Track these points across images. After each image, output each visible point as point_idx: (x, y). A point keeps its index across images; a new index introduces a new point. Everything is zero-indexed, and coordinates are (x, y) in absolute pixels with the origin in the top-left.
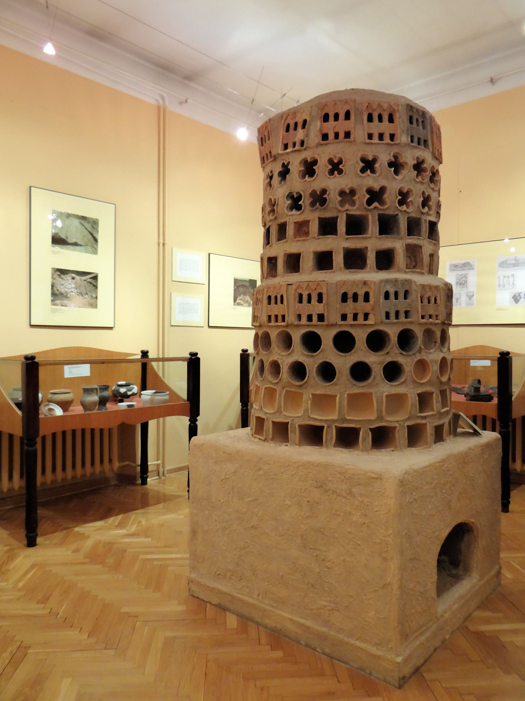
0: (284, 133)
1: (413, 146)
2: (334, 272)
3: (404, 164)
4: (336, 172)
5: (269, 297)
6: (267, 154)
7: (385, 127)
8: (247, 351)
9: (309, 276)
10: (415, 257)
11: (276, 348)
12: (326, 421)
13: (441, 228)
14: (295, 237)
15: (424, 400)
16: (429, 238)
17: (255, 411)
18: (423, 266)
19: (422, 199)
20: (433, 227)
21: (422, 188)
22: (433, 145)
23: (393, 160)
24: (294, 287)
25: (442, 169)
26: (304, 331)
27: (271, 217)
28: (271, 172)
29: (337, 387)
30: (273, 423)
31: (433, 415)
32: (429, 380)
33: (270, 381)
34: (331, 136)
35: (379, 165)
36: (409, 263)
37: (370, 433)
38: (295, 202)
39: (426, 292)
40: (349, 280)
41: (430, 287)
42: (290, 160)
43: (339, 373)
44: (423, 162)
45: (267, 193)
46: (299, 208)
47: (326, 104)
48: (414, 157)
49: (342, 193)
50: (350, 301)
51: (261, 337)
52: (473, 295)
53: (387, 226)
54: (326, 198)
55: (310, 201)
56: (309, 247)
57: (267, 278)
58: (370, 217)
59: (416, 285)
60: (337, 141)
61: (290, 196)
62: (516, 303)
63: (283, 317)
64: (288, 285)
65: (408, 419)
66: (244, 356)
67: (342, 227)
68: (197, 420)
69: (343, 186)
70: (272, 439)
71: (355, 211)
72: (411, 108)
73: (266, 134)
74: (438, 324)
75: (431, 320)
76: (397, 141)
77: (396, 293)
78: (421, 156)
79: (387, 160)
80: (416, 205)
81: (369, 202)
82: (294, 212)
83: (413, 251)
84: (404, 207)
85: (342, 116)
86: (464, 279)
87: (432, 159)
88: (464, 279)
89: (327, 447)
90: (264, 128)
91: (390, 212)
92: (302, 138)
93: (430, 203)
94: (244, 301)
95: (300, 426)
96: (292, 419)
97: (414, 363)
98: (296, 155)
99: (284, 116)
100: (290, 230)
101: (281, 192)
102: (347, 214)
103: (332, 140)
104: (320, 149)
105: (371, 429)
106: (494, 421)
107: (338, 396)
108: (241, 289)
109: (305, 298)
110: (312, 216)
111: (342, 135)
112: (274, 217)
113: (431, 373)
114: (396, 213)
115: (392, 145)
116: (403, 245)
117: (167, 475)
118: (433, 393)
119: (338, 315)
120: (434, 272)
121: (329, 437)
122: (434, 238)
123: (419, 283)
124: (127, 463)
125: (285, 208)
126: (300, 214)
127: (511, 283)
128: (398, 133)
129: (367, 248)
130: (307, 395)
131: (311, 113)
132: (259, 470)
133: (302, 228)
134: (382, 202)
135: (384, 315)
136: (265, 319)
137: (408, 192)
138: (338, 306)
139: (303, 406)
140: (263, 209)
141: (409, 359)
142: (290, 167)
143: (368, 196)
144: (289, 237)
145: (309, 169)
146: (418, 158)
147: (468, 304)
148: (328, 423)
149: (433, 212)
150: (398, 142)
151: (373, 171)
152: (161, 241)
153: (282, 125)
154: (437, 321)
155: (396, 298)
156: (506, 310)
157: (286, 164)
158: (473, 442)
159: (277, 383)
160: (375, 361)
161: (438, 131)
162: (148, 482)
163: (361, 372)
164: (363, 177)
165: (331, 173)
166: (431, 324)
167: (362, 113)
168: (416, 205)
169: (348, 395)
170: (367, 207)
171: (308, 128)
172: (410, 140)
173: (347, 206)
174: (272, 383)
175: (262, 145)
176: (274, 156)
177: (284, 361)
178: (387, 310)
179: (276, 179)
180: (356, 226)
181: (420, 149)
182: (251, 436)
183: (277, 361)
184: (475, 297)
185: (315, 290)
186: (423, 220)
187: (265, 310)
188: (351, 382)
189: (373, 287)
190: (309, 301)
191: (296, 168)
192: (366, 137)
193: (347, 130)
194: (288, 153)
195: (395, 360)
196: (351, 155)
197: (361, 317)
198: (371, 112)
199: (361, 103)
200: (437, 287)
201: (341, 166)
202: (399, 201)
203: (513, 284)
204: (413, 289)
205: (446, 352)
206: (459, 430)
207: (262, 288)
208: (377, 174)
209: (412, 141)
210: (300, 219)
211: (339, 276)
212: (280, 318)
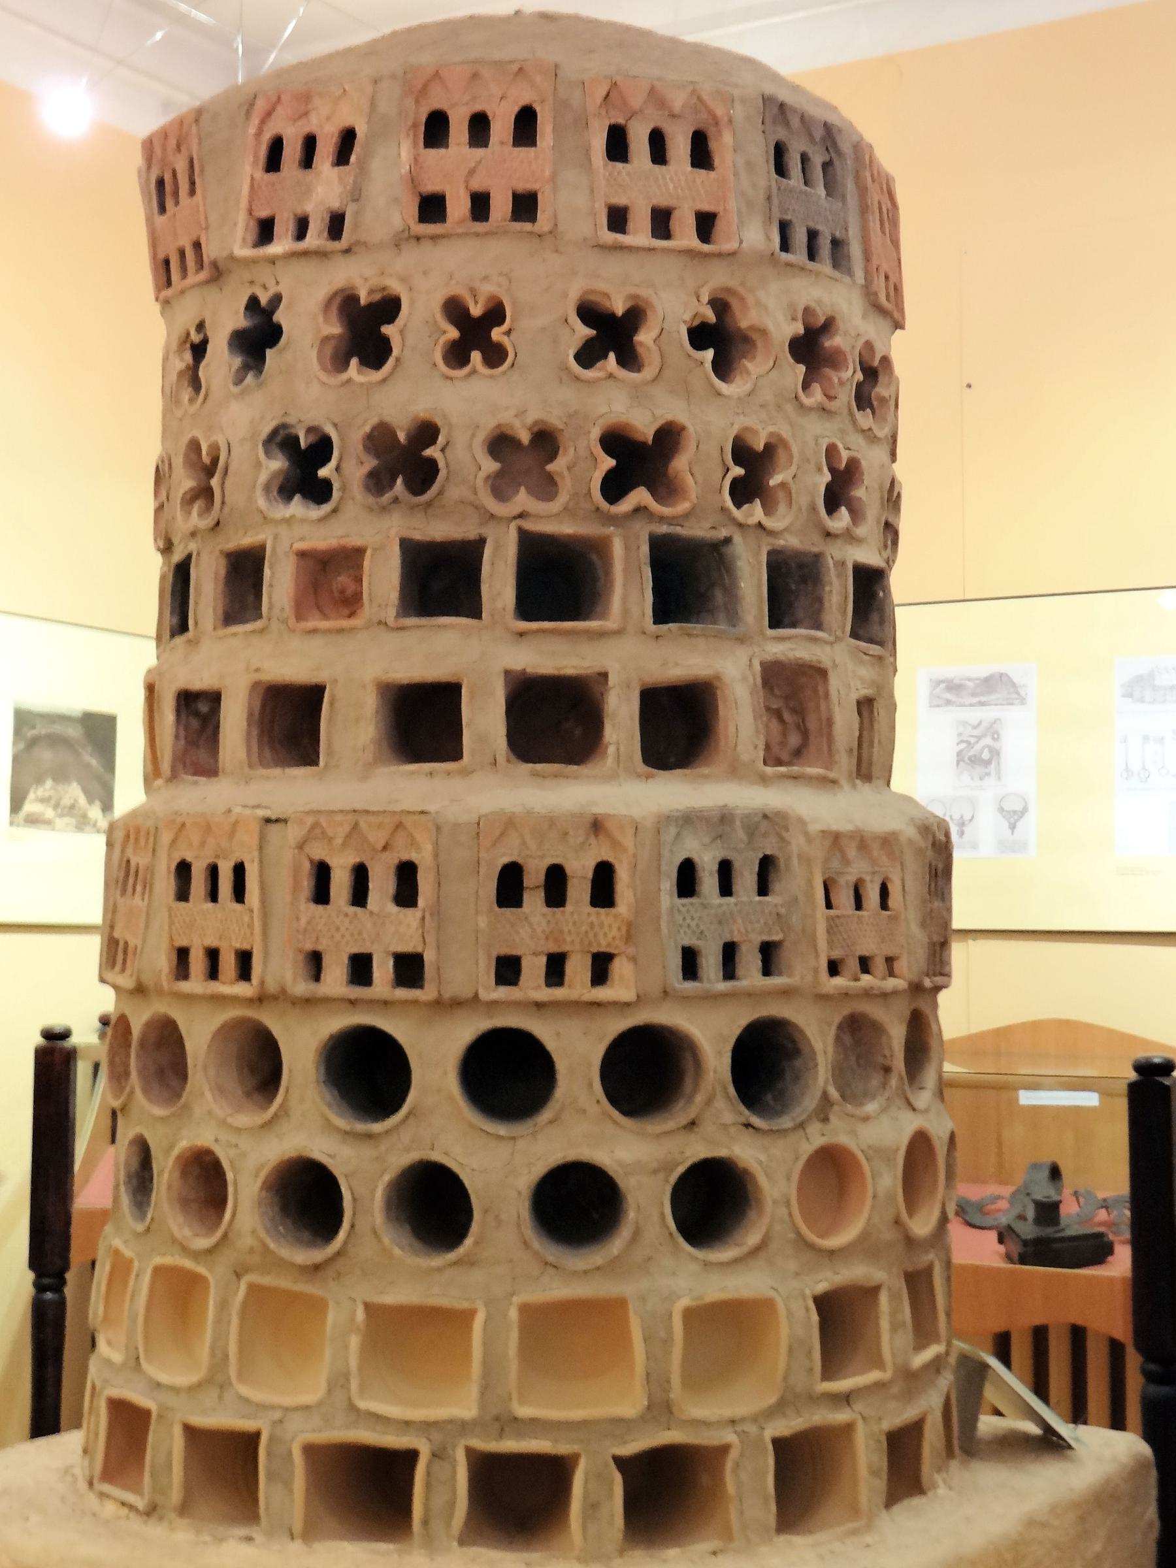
0: (260, 174)
1: (789, 265)
2: (466, 773)
3: (755, 336)
4: (476, 356)
5: (183, 870)
6: (182, 253)
7: (679, 185)
8: (65, 1035)
9: (356, 786)
10: (800, 712)
11: (208, 1095)
12: (427, 1427)
13: (900, 584)
14: (299, 617)
15: (840, 1319)
16: (854, 635)
17: (108, 1367)
19: (827, 477)
20: (869, 585)
22: (867, 258)
24: (293, 833)
25: (903, 351)
27: (196, 519)
28: (200, 326)
29: (477, 1276)
30: (192, 1433)
31: (880, 1386)
32: (864, 1237)
33: (174, 1241)
34: (458, 207)
35: (654, 333)
36: (776, 738)
37: (618, 1478)
38: (304, 467)
39: (846, 861)
40: (529, 813)
41: (862, 841)
42: (283, 289)
43: (486, 1212)
44: (828, 326)
45: (179, 413)
46: (319, 492)
47: (437, 75)
48: (792, 306)
49: (501, 444)
50: (534, 900)
51: (143, 1043)
52: (1025, 810)
53: (685, 583)
56: (366, 657)
57: (174, 777)
58: (618, 549)
59: (806, 834)
60: (480, 227)
61: (282, 440)
63: (244, 960)
64: (268, 821)
65: (779, 1408)
66: (54, 1063)
67: (499, 581)
70: (185, 1508)
71: (555, 519)
72: (777, 110)
73: (181, 167)
74: (895, 993)
75: (866, 978)
76: (723, 242)
77: (725, 870)
78: (819, 302)
79: (687, 317)
80: (803, 501)
81: (614, 487)
82: (298, 507)
83: (792, 693)
84: (755, 512)
86: (987, 741)
87: (865, 316)
88: (987, 741)
89: (429, 1543)
90: (172, 142)
91: (698, 530)
92: (336, 205)
93: (859, 493)
94: (56, 806)
95: (310, 1450)
96: (277, 1415)
97: (800, 1165)
98: (306, 270)
99: (261, 105)
100: (280, 583)
101: (241, 418)
102: (523, 535)
103: (461, 222)
104: (410, 259)
105: (620, 1462)
106: (1116, 1349)
108: (46, 755)
109: (341, 883)
110: (377, 532)
111: (501, 206)
112: (209, 522)
113: (869, 1201)
114: (723, 533)
115: (706, 256)
116: (751, 665)
119: (483, 963)
120: (876, 770)
121: (439, 1501)
122: (875, 629)
123: (820, 827)
129: (604, 676)
130: (343, 1309)
131: (373, 105)
133: (330, 579)
134: (663, 486)
135: (675, 961)
136: (162, 962)
137: (769, 449)
138: (483, 922)
139: (328, 1353)
140: (160, 477)
141: (780, 1150)
142: (280, 317)
143: (611, 463)
144: (276, 612)
145: (365, 331)
148: (437, 1436)
149: (869, 528)
151: (629, 359)
153: (250, 140)
154: (892, 983)
155: (726, 888)
157: (264, 300)
158: (1043, 1486)
159: (210, 1252)
160: (640, 1157)
161: (886, 204)
163: (576, 1205)
164: (588, 382)
165: (457, 355)
166: (867, 994)
167: (582, 123)
170: (604, 505)
171: (363, 170)
173: (523, 500)
174: (185, 1250)
175: (162, 209)
176: (215, 265)
177: (244, 1155)
178: (687, 942)
179: (221, 360)
180: (558, 582)
181: (818, 274)
182: (82, 1485)
183: (208, 1152)
184: (1031, 817)
185: (385, 848)
187: (163, 923)
188: (536, 1253)
189: (628, 841)
190: (359, 896)
191: (307, 324)
192: (604, 220)
193: (522, 186)
194: (272, 261)
195: (721, 1152)
196: (541, 290)
197: (578, 969)
198: (621, 121)
200: (888, 841)
201: (496, 334)
202: (735, 483)
205: (927, 1111)
206: (987, 1424)
207: (150, 824)
208: (648, 373)
209: (785, 246)
210: (324, 538)
211: (489, 794)
212: (228, 963)
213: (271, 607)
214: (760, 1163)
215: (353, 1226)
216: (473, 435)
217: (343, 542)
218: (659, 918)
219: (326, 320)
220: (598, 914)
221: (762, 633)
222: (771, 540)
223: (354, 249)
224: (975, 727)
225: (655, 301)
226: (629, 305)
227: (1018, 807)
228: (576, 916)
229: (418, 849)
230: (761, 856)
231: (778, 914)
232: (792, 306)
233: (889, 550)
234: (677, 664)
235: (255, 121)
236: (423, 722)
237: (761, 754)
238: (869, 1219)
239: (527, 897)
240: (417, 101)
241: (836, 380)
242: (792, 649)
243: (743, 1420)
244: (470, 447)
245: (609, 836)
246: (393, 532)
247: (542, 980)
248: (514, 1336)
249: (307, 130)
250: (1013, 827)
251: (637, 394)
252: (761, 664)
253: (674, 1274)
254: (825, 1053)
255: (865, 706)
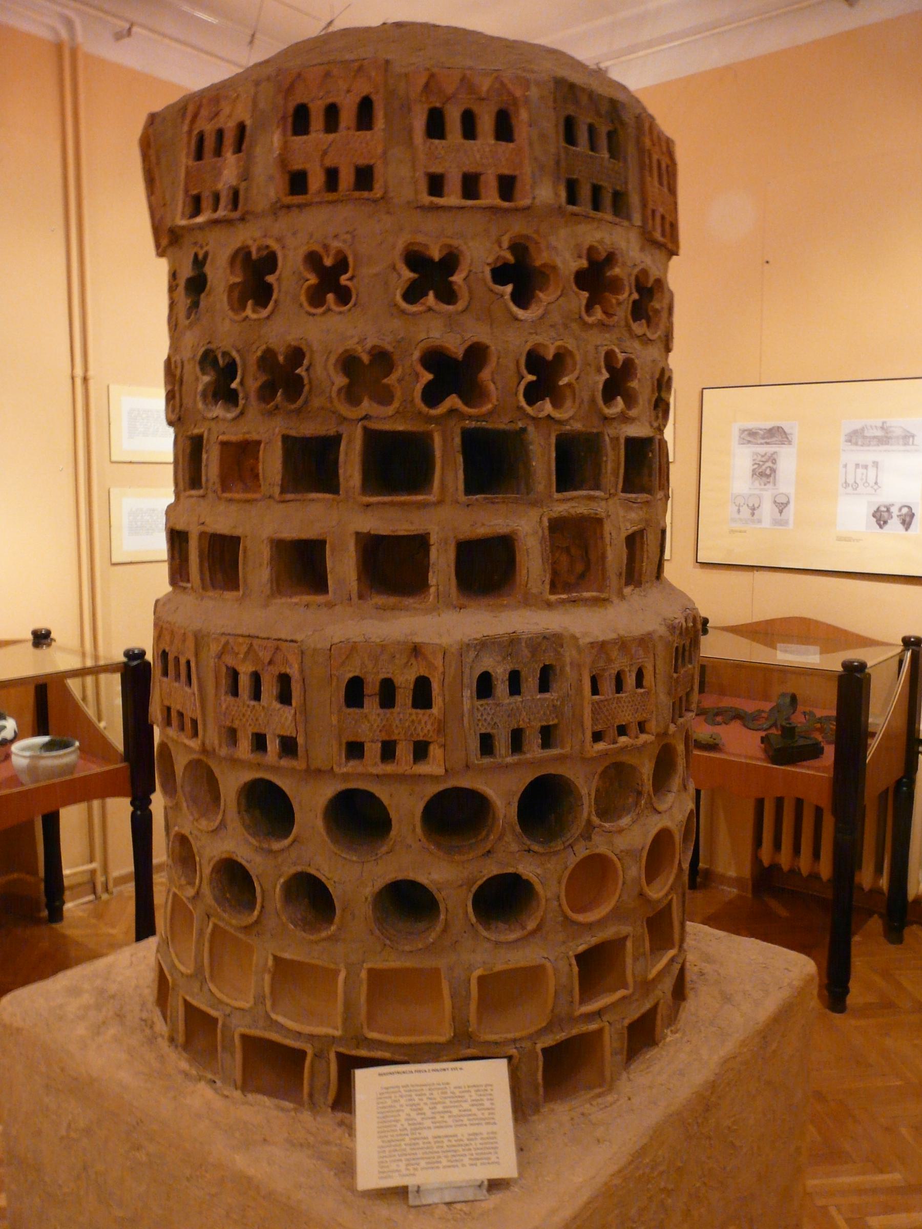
0: (191, 163)
1: (574, 214)
2: (330, 605)
4: (330, 297)
7: (485, 154)
12: (311, 1037)
14: (225, 488)
18: (604, 577)
19: (606, 375)
21: (603, 341)
22: (644, 205)
23: (510, 258)
26: (249, 776)
32: (616, 909)
34: (316, 181)
35: (463, 275)
39: (610, 661)
41: (623, 644)
43: (344, 910)
44: (611, 259)
47: (299, 75)
48: (578, 246)
49: (349, 363)
50: (371, 706)
52: (788, 503)
54: (300, 378)
55: (258, 384)
60: (331, 196)
62: (881, 527)
67: (350, 467)
68: (150, 802)
69: (351, 344)
71: (388, 419)
81: (432, 396)
84: (547, 407)
85: (347, 117)
86: (769, 464)
87: (642, 249)
89: (313, 1105)
91: (502, 424)
96: (228, 1010)
97: (567, 873)
99: (191, 109)
102: (365, 429)
104: (281, 225)
106: (819, 811)
107: (342, 976)
109: (244, 682)
111: (346, 178)
115: (506, 210)
117: (115, 891)
118: (625, 938)
123: (588, 640)
124: (15, 876)
125: (198, 398)
126: (235, 419)
127: (872, 481)
128: (526, 173)
130: (263, 953)
132: (138, 1148)
134: (472, 392)
135: (474, 744)
143: (428, 377)
146: (591, 250)
147: (776, 522)
150: (527, 202)
151: (448, 295)
152: (79, 371)
153: (185, 139)
156: (858, 540)
162: (66, 914)
163: (408, 902)
166: (623, 749)
167: (406, 108)
168: (586, 396)
169: (370, 971)
170: (425, 409)
172: (563, 195)
173: (367, 406)
181: (601, 220)
184: (792, 506)
185: (270, 663)
186: (607, 439)
189: (438, 662)
190: (256, 695)
192: (423, 186)
193: (362, 162)
194: (201, 227)
196: (376, 241)
197: (404, 751)
199: (406, 75)
200: (644, 641)
201: (344, 280)
203: (876, 483)
204: (568, 660)
208: (461, 305)
209: (572, 199)
213: (207, 480)
214: (538, 876)
215: (263, 907)
216: (328, 358)
217: (247, 436)
218: (463, 716)
219: (232, 273)
220: (417, 714)
221: (550, 497)
222: (557, 427)
223: (248, 217)
224: (763, 456)
225: (463, 248)
226: (444, 252)
227: (785, 501)
228: (401, 716)
229: (291, 667)
230: (541, 665)
231: (554, 706)
232: (578, 246)
233: (660, 420)
234: (483, 525)
235: (187, 121)
236: (303, 565)
237: (548, 587)
238: (620, 896)
239: (366, 701)
240: (286, 98)
241: (614, 301)
242: (573, 507)
243: (521, 1039)
244: (325, 368)
245: (425, 658)
246: (277, 430)
247: (378, 759)
248: (364, 988)
249: (218, 126)
250: (781, 512)
251: (451, 322)
252: (550, 520)
253: (474, 951)
254: (589, 795)
255: (633, 541)
